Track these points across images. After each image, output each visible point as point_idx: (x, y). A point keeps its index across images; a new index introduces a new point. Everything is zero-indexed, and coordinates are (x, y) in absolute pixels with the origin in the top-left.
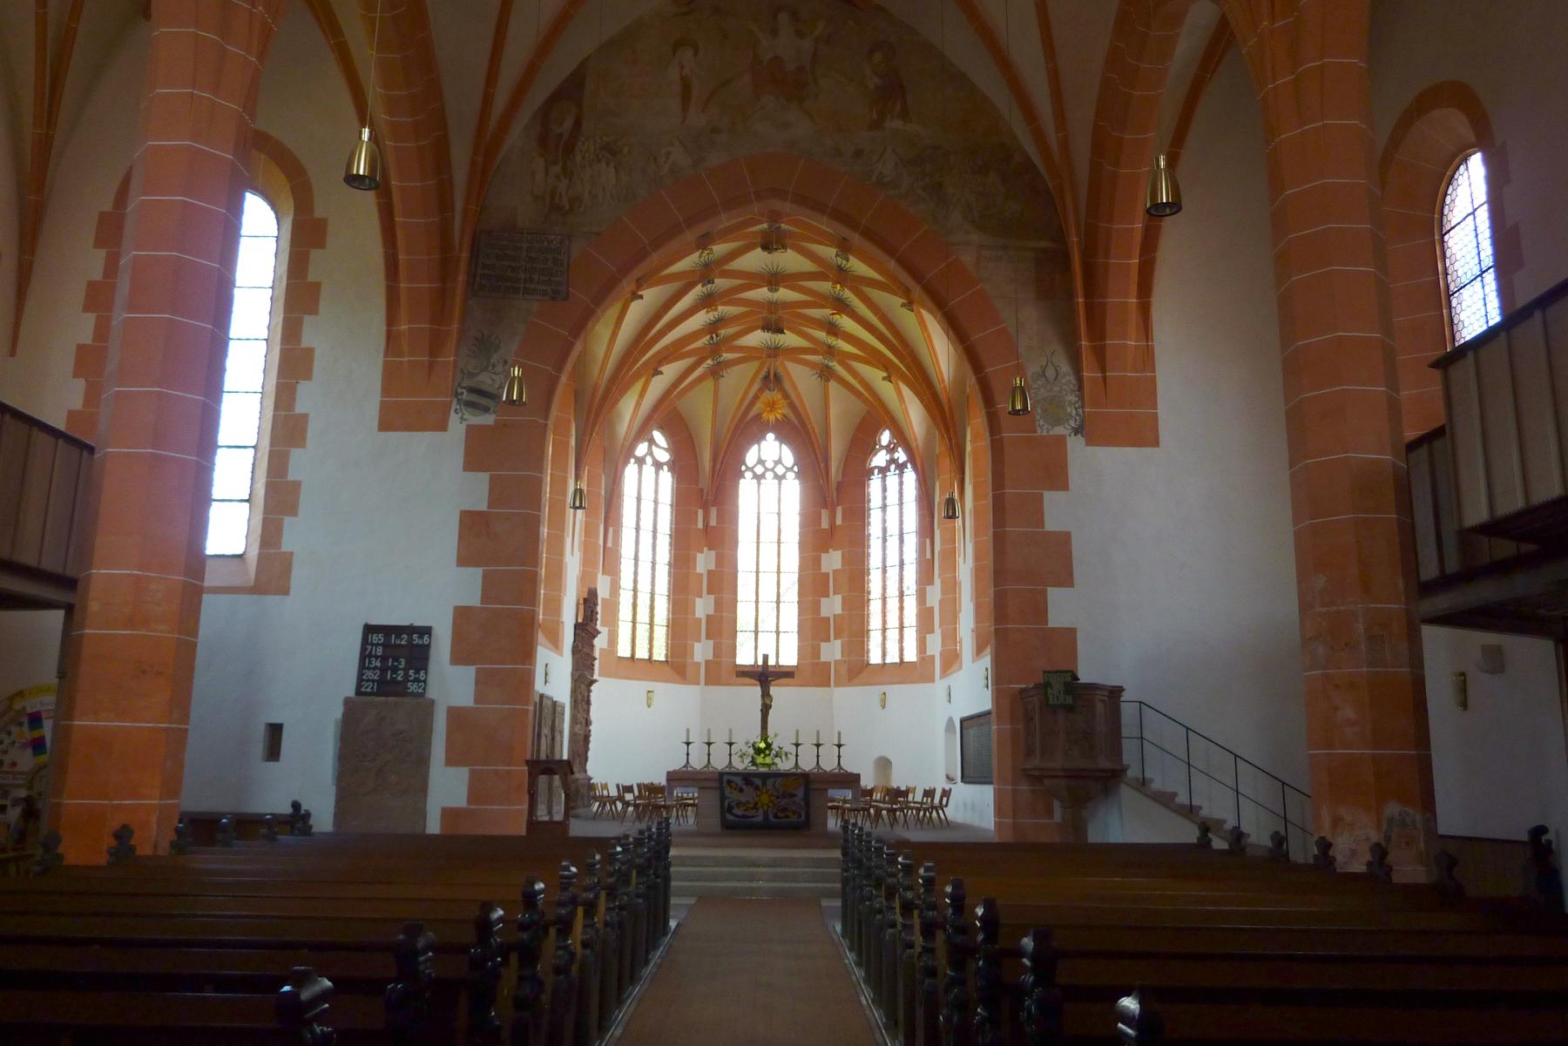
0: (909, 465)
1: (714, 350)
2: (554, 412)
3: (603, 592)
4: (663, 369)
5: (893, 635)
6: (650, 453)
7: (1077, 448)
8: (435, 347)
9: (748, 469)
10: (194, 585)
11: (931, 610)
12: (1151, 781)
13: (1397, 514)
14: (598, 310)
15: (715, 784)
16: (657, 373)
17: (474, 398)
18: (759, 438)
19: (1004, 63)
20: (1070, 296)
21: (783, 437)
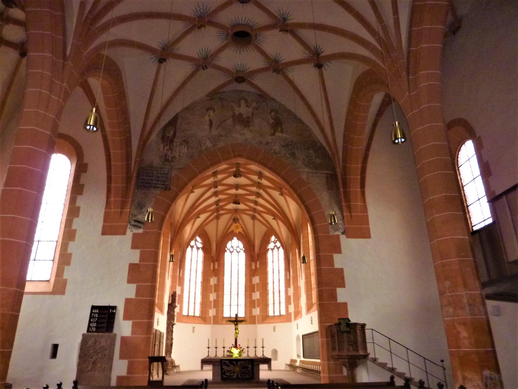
0: (281, 247)
1: (217, 210)
2: (164, 228)
3: (178, 292)
4: (200, 216)
5: (277, 305)
6: (196, 245)
7: (343, 239)
8: (123, 205)
10: (20, 291)
11: (290, 296)
12: (378, 359)
13: (473, 258)
14: (180, 193)
15: (219, 364)
16: (198, 217)
17: (136, 224)
18: (231, 239)
19: (313, 114)
20: (338, 188)
21: (238, 239)
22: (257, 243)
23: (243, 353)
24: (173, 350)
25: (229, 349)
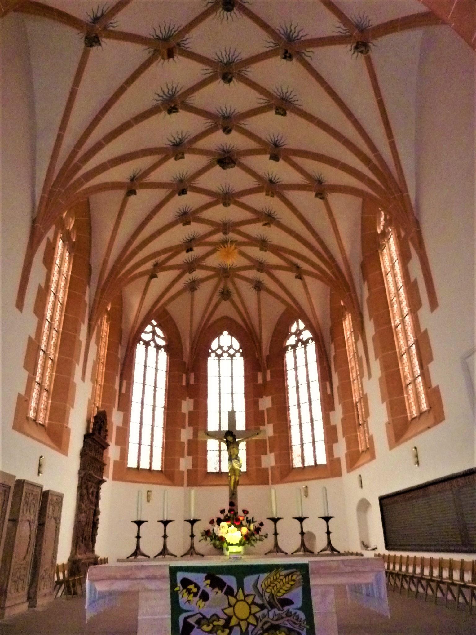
6: (153, 340)
9: (213, 351)
11: (334, 428)
18: (218, 334)
21: (231, 334)
22: (266, 336)
23: (261, 540)
24: (98, 538)
25: (209, 527)
